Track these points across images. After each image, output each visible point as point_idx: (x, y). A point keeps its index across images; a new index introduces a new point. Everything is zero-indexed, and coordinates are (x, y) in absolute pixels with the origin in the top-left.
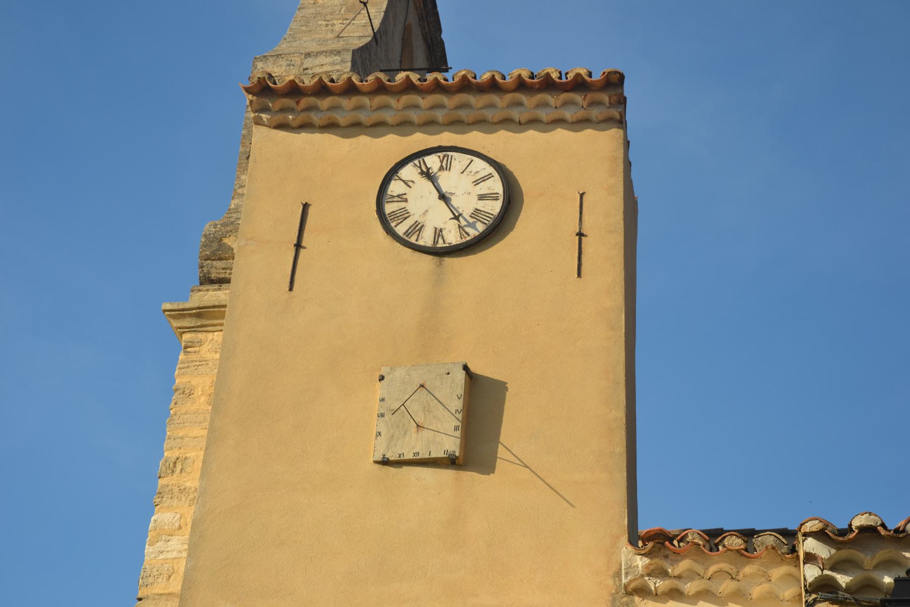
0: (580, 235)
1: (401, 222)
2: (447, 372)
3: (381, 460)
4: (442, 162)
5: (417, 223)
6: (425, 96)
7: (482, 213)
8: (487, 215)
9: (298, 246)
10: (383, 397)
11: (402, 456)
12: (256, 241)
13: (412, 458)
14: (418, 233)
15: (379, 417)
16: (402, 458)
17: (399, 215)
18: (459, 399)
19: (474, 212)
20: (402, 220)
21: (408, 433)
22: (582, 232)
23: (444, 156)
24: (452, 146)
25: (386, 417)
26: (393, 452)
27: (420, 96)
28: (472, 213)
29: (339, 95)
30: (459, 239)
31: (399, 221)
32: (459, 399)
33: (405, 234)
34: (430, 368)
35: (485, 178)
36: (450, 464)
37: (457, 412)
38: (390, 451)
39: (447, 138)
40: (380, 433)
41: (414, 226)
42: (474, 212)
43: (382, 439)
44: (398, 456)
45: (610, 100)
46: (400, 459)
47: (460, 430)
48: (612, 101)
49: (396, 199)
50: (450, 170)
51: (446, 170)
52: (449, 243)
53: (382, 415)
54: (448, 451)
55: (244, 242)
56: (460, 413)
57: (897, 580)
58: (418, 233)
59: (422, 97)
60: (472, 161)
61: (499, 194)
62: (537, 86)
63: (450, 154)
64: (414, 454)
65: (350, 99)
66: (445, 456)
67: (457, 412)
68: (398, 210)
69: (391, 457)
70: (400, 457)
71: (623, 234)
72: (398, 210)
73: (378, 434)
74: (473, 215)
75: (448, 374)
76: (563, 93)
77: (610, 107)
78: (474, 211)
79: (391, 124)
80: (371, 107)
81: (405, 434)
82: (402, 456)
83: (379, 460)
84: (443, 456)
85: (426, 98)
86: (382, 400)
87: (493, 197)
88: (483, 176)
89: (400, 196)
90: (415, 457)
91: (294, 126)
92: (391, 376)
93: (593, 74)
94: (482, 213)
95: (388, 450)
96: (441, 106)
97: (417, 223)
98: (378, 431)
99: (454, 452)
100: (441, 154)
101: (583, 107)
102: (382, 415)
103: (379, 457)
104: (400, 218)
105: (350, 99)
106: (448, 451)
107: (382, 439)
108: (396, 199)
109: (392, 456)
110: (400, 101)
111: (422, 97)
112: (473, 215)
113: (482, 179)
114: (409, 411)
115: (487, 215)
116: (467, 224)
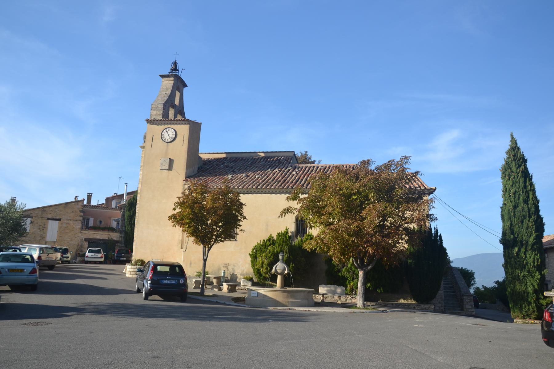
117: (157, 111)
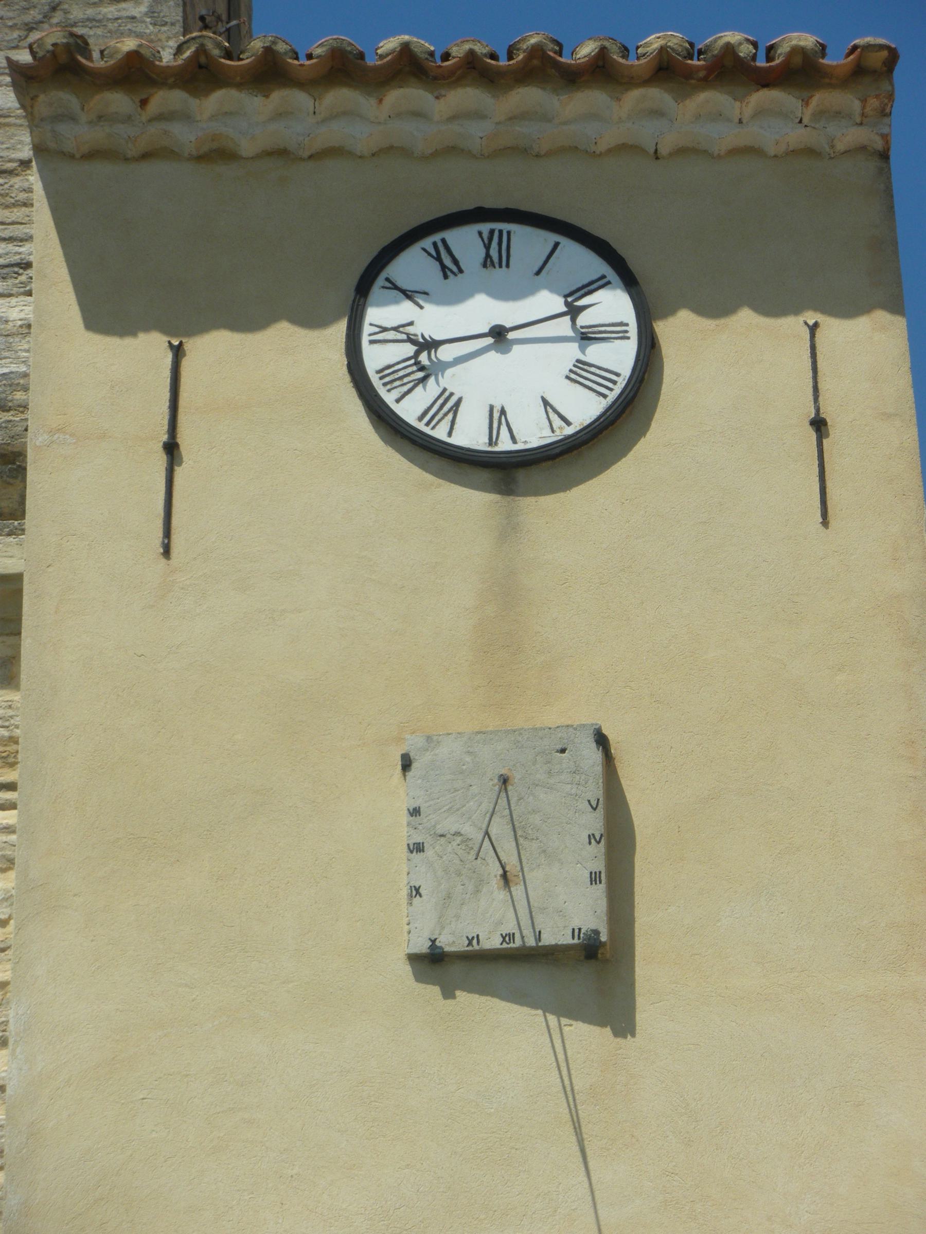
0: (819, 425)
1: (410, 391)
2: (559, 747)
3: (428, 951)
4: (487, 247)
5: (447, 394)
6: (443, 92)
7: (593, 369)
8: (598, 372)
9: (171, 448)
10: (416, 805)
11: (475, 942)
12: (72, 435)
13: (499, 946)
14: (450, 416)
15: (412, 852)
16: (476, 947)
17: (401, 373)
18: (595, 809)
19: (575, 369)
20: (411, 385)
21: (484, 890)
22: (823, 416)
23: (492, 232)
24: (507, 209)
25: (429, 853)
26: (453, 933)
27: (432, 93)
28: (571, 371)
29: (239, 86)
30: (547, 432)
31: (405, 388)
32: (595, 809)
33: (420, 419)
34: (520, 739)
35: (592, 287)
36: (582, 958)
37: (593, 841)
38: (445, 931)
39: (118, 40)
40: (417, 890)
41: (440, 401)
42: (575, 369)
43: (426, 905)
44: (467, 942)
45: (864, 108)
46: (470, 948)
47: (603, 882)
48: (868, 109)
49: (391, 335)
50: (508, 266)
51: (501, 266)
52: (525, 442)
53: (418, 848)
54: (580, 929)
55: (46, 436)
56: (599, 842)
57: (15, 635)
58: (450, 416)
59: (436, 94)
60: (557, 245)
61: (627, 325)
62: (702, 74)
63: (505, 227)
64: (504, 938)
65: (267, 96)
66: (576, 941)
67: (593, 841)
68: (398, 363)
69: (449, 945)
70: (470, 944)
71: (914, 420)
72: (398, 363)
73: (414, 893)
74: (573, 376)
75: (563, 751)
76: (758, 90)
77: (861, 124)
78: (575, 366)
79: (359, 154)
80: (314, 113)
81: (477, 891)
82: (475, 942)
83: (424, 951)
84: (571, 941)
85: (445, 96)
86: (415, 812)
87: (616, 332)
88: (586, 281)
89: (401, 329)
90: (505, 945)
91: (130, 154)
92: (428, 757)
93: (827, 51)
94: (593, 369)
95: (443, 928)
96: (479, 115)
97: (447, 394)
98: (412, 884)
99: (596, 932)
100: (485, 227)
101: (801, 122)
102: (418, 848)
103: (422, 946)
104: (405, 380)
105: (267, 96)
106: (580, 929)
107: (426, 905)
108: (391, 335)
109: (451, 942)
110: (384, 102)
111: (436, 94)
112: (573, 376)
113: (586, 290)
114: (523, 857)
115: (598, 372)
116: (381, 329)
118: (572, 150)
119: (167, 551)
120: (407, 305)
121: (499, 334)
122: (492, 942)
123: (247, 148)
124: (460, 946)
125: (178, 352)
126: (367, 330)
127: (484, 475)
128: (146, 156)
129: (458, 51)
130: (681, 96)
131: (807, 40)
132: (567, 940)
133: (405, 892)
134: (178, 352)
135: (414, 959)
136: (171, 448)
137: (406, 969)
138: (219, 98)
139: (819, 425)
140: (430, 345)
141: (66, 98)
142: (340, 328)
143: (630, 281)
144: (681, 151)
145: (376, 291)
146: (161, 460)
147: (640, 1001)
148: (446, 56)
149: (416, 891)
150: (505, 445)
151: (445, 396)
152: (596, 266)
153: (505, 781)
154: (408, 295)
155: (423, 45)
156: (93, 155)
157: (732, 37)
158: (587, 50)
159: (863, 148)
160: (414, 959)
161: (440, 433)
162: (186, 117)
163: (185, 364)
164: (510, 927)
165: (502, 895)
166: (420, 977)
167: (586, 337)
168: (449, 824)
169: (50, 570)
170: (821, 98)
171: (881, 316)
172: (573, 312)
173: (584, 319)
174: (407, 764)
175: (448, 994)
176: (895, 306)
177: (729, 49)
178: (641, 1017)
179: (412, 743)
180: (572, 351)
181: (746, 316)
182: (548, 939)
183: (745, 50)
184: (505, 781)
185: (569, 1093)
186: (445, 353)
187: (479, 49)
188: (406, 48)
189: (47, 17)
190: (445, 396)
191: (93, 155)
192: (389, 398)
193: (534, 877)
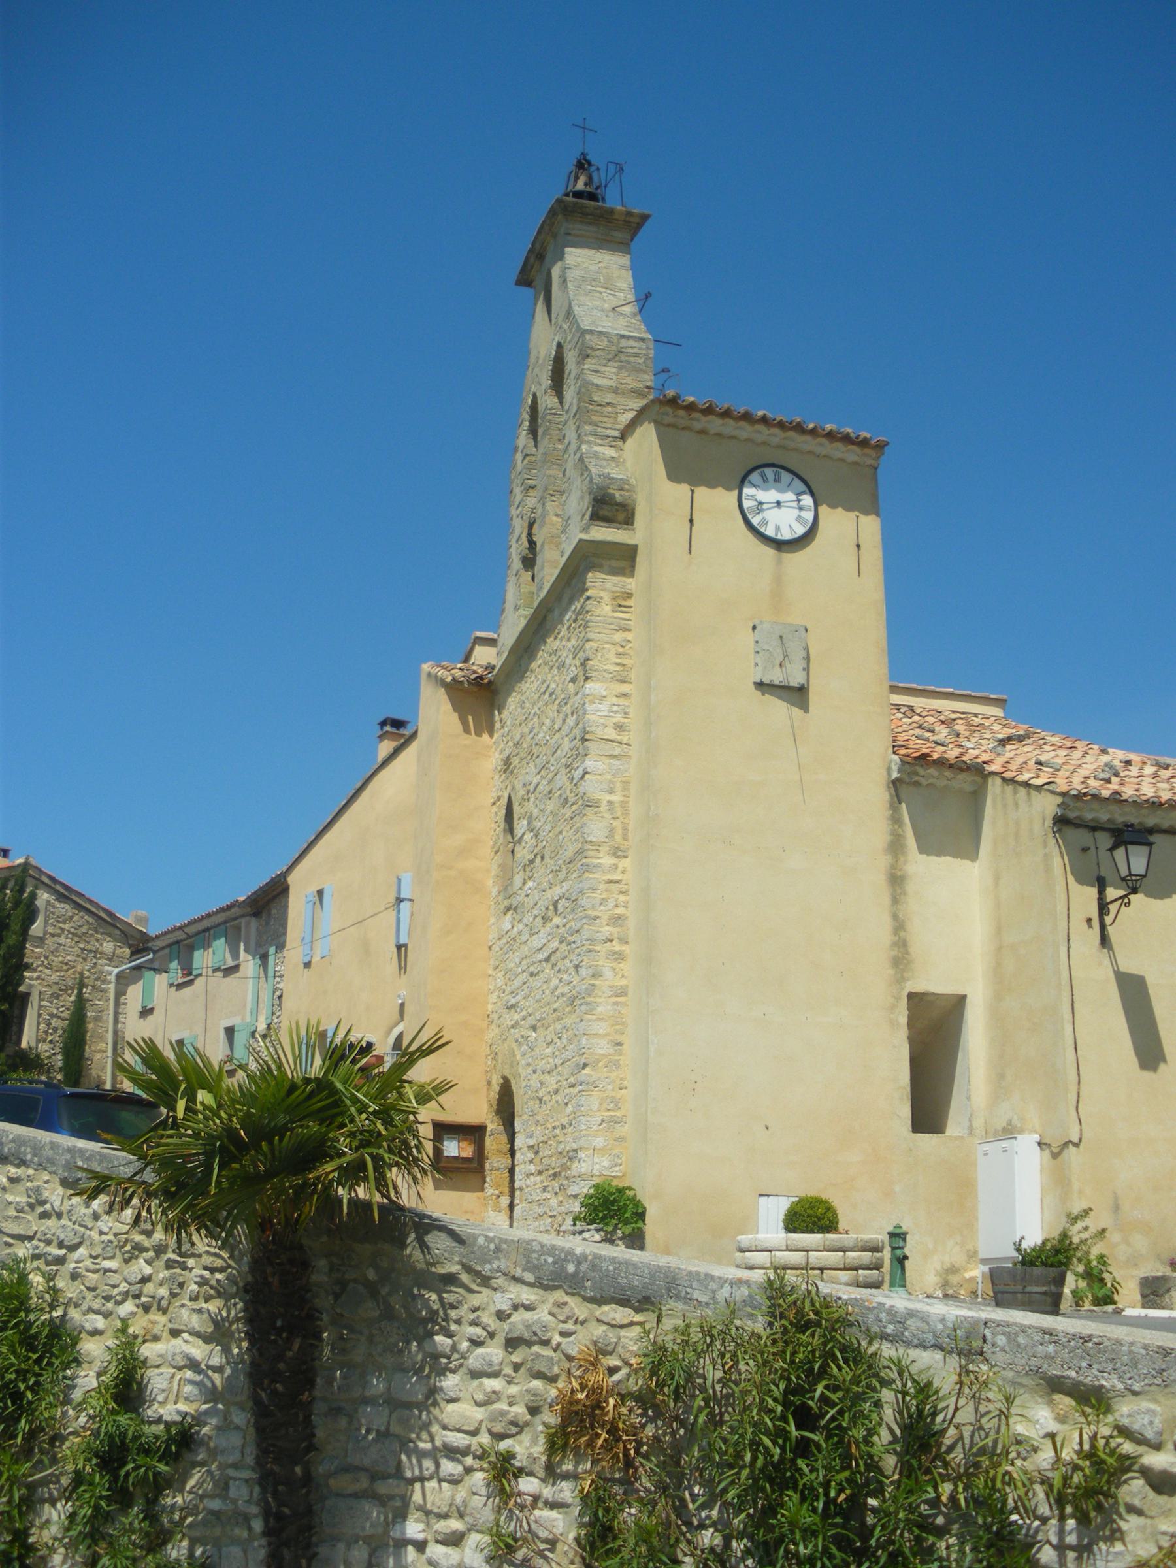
0: (858, 546)
9: (691, 521)
53: (758, 652)
96: (775, 436)
102: (758, 652)
103: (758, 680)
109: (766, 680)
117: (620, 368)
118: (796, 450)
119: (690, 553)
120: (754, 489)
121: (778, 503)
122: (777, 682)
123: (712, 431)
124: (768, 682)
125: (693, 492)
126: (744, 495)
127: (773, 545)
128: (683, 428)
129: (778, 419)
130: (831, 442)
131: (868, 435)
132: (796, 685)
133: (753, 664)
134: (693, 492)
135: (755, 683)
136: (691, 521)
137: (752, 686)
138: (711, 417)
139: (858, 546)
140: (761, 503)
141: (669, 409)
142: (736, 492)
143: (812, 494)
144: (824, 456)
145: (746, 483)
146: (688, 524)
147: (811, 704)
148: (775, 420)
149: (756, 665)
150: (779, 537)
151: (764, 519)
152: (803, 487)
153: (781, 637)
154: (755, 486)
155: (770, 415)
156: (669, 425)
157: (849, 430)
158: (811, 426)
159: (871, 465)
160: (755, 683)
161: (762, 530)
162: (698, 420)
163: (695, 495)
164: (781, 679)
165: (779, 670)
166: (756, 689)
167: (801, 509)
168: (766, 647)
169: (988, 755)
170: (867, 451)
171: (874, 517)
172: (799, 501)
173: (801, 503)
174: (754, 628)
175: (763, 695)
176: (878, 514)
177: (848, 434)
178: (810, 708)
179: (756, 622)
180: (797, 512)
181: (840, 510)
182: (792, 684)
183: (852, 435)
184: (781, 637)
185: (793, 727)
186: (765, 506)
187: (784, 420)
188: (765, 415)
189: (614, 358)
190: (764, 519)
191: (669, 425)
192: (750, 517)
193: (788, 666)
